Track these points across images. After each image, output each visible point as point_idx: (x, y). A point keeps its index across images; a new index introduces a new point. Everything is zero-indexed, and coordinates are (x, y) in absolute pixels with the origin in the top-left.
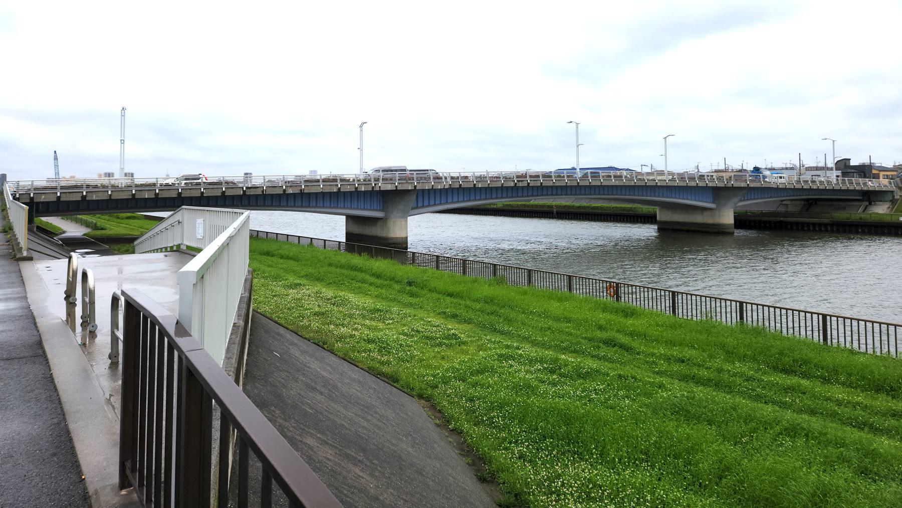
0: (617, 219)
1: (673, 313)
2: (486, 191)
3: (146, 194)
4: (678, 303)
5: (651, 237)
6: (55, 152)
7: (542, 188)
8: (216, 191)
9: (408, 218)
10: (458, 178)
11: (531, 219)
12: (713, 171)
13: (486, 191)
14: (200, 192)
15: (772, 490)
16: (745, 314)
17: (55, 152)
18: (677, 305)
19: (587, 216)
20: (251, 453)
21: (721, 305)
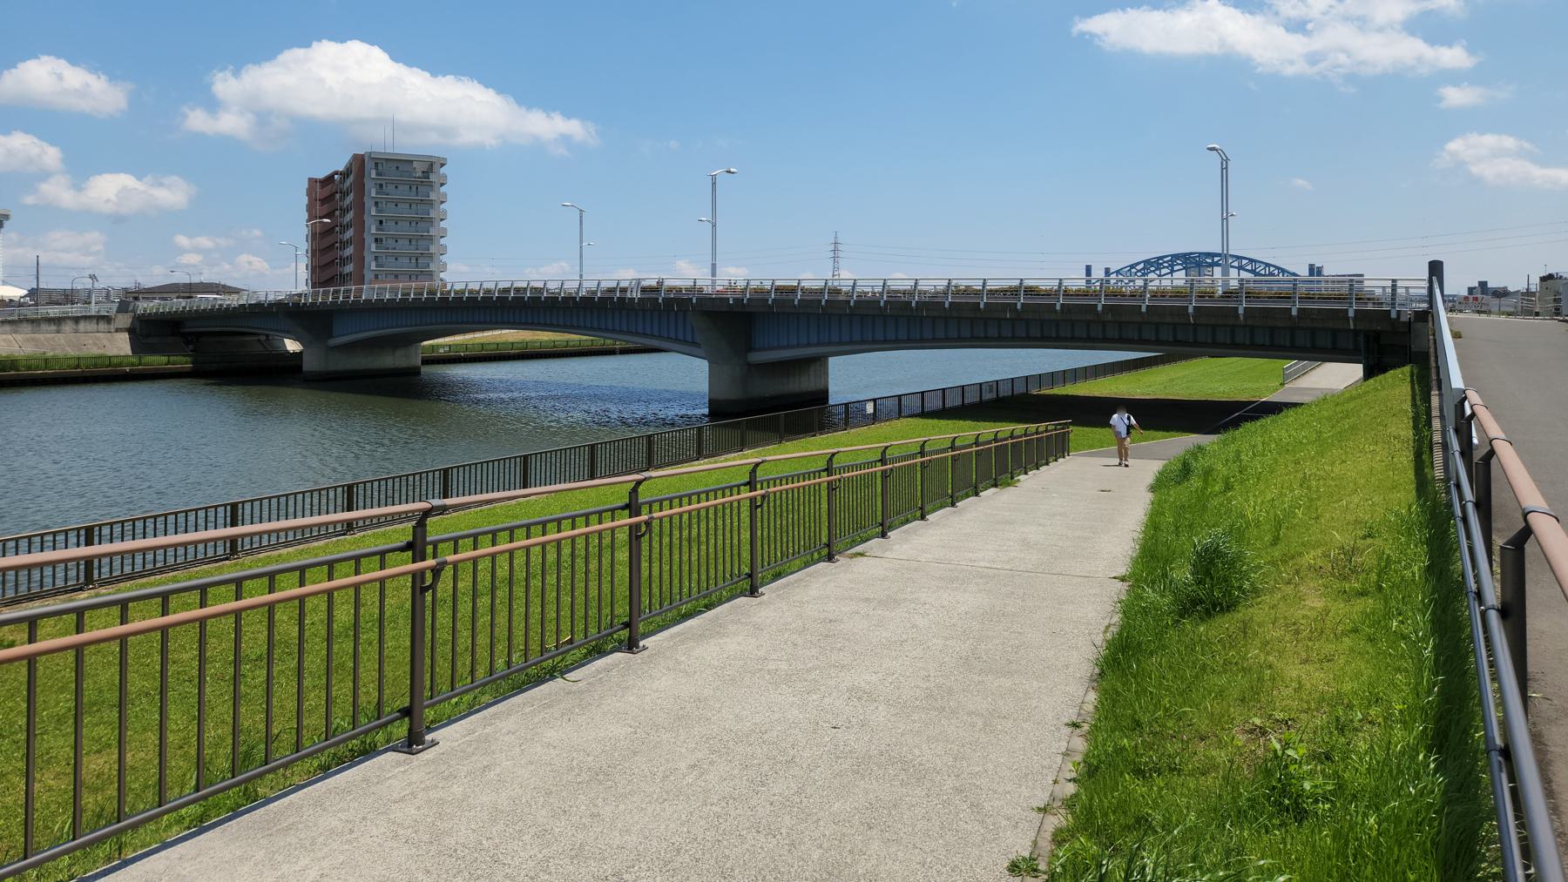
9: (831, 359)
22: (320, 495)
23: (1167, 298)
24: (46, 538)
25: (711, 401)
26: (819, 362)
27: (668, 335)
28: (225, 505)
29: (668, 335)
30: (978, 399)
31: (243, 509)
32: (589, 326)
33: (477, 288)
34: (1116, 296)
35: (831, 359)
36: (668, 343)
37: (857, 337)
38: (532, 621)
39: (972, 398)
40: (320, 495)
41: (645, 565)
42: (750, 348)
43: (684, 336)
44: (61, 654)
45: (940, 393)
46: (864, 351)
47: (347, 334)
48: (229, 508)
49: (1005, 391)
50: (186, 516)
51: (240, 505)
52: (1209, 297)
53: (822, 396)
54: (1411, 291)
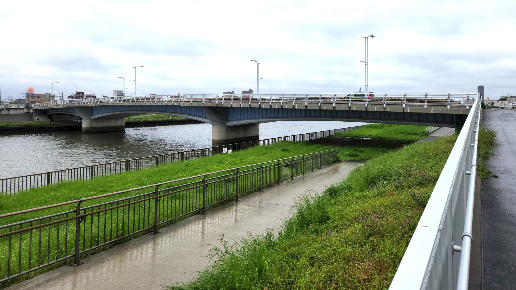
0: (133, 126)
1: (91, 176)
2: (247, 111)
3: (432, 109)
4: (89, 171)
5: (402, 133)
6: (360, 88)
7: (251, 109)
8: (397, 107)
9: (260, 124)
10: (446, 101)
11: (188, 125)
12: (13, 101)
13: (247, 111)
14: (365, 107)
15: (510, 234)
16: (50, 178)
17: (360, 88)
18: (90, 170)
19: (134, 125)
20: (83, 222)
21: (100, 171)
22: (65, 172)
23: (379, 101)
24: (119, 163)
25: (212, 140)
26: (255, 125)
27: (200, 115)
28: (45, 173)
29: (205, 116)
30: (316, 138)
31: (95, 168)
32: (174, 112)
33: (319, 96)
34: (378, 101)
35: (261, 125)
36: (194, 117)
37: (272, 116)
38: (100, 229)
39: (314, 137)
40: (65, 172)
41: (239, 184)
42: (227, 120)
43: (203, 116)
44: (65, 205)
45: (339, 130)
46: (281, 121)
47: (96, 115)
48: (46, 174)
49: (320, 136)
50: (78, 170)
51: (94, 167)
52: (394, 101)
53: (258, 137)
54: (10, 124)
